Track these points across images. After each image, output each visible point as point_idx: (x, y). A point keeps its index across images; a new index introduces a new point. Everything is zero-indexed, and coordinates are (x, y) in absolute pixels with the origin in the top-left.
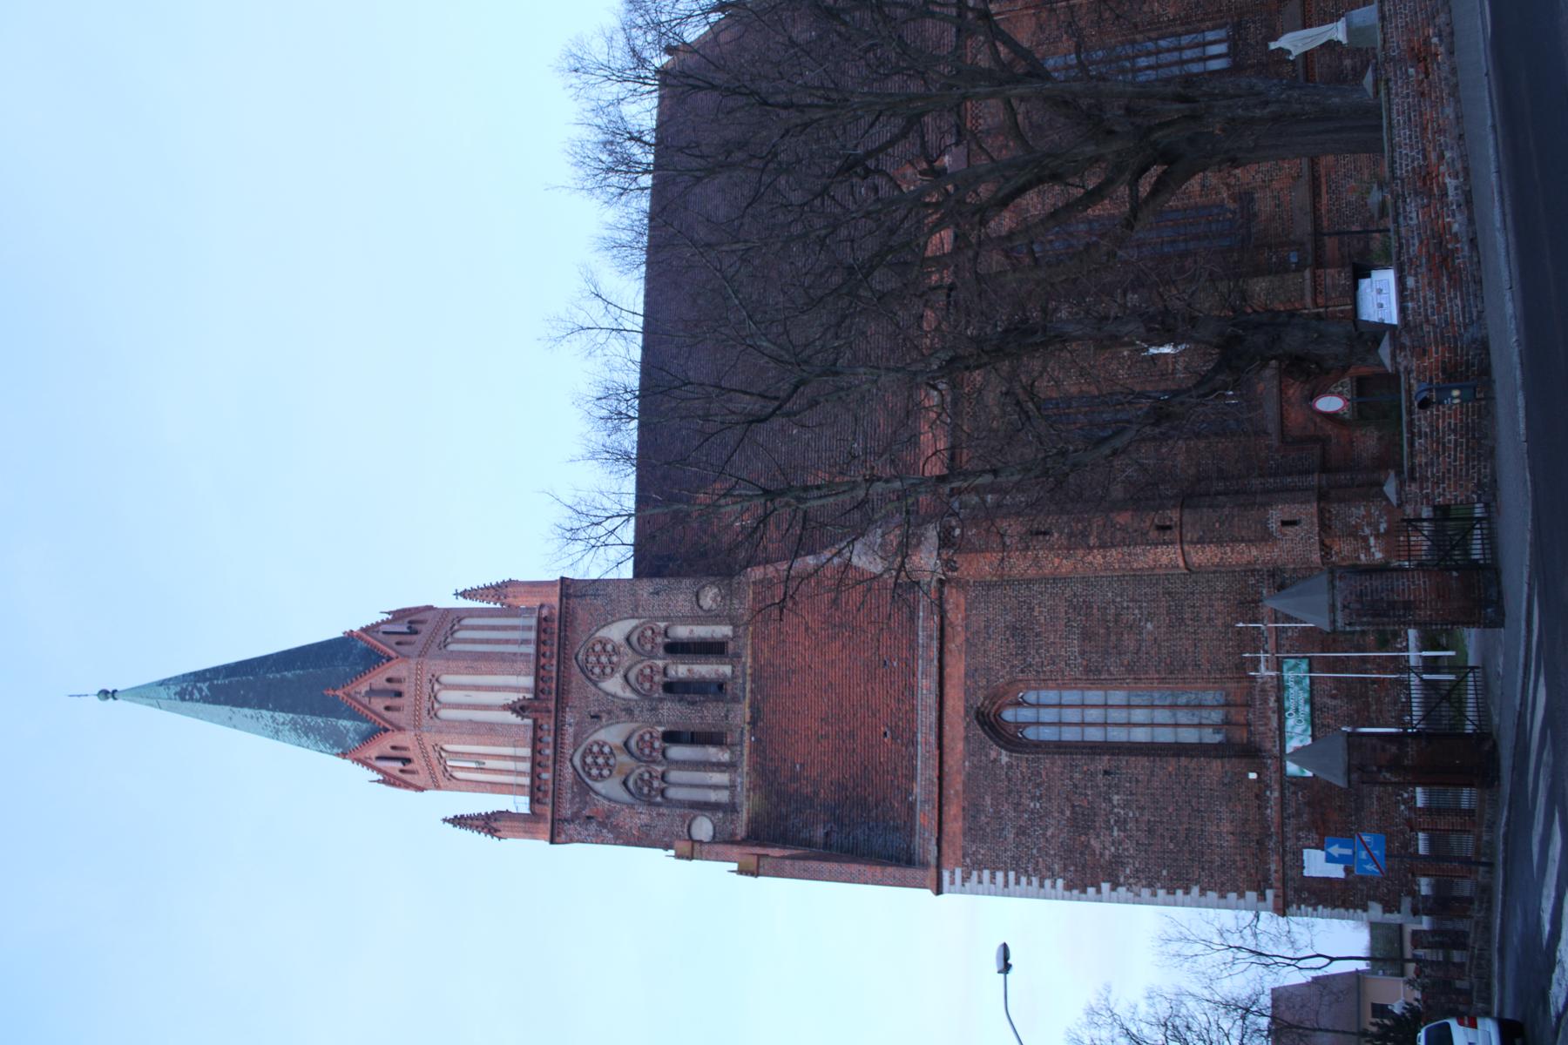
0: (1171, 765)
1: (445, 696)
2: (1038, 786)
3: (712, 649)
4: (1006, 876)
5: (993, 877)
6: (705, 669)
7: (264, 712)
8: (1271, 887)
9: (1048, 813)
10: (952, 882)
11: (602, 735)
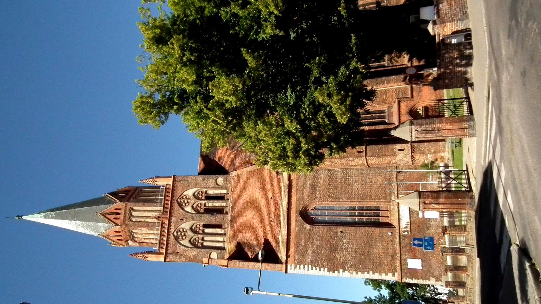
0: (363, 229)
1: (134, 214)
2: (319, 236)
3: (220, 198)
4: (308, 266)
5: (304, 267)
6: (217, 204)
7: (73, 221)
8: (397, 272)
9: (322, 245)
10: (291, 269)
11: (183, 226)
